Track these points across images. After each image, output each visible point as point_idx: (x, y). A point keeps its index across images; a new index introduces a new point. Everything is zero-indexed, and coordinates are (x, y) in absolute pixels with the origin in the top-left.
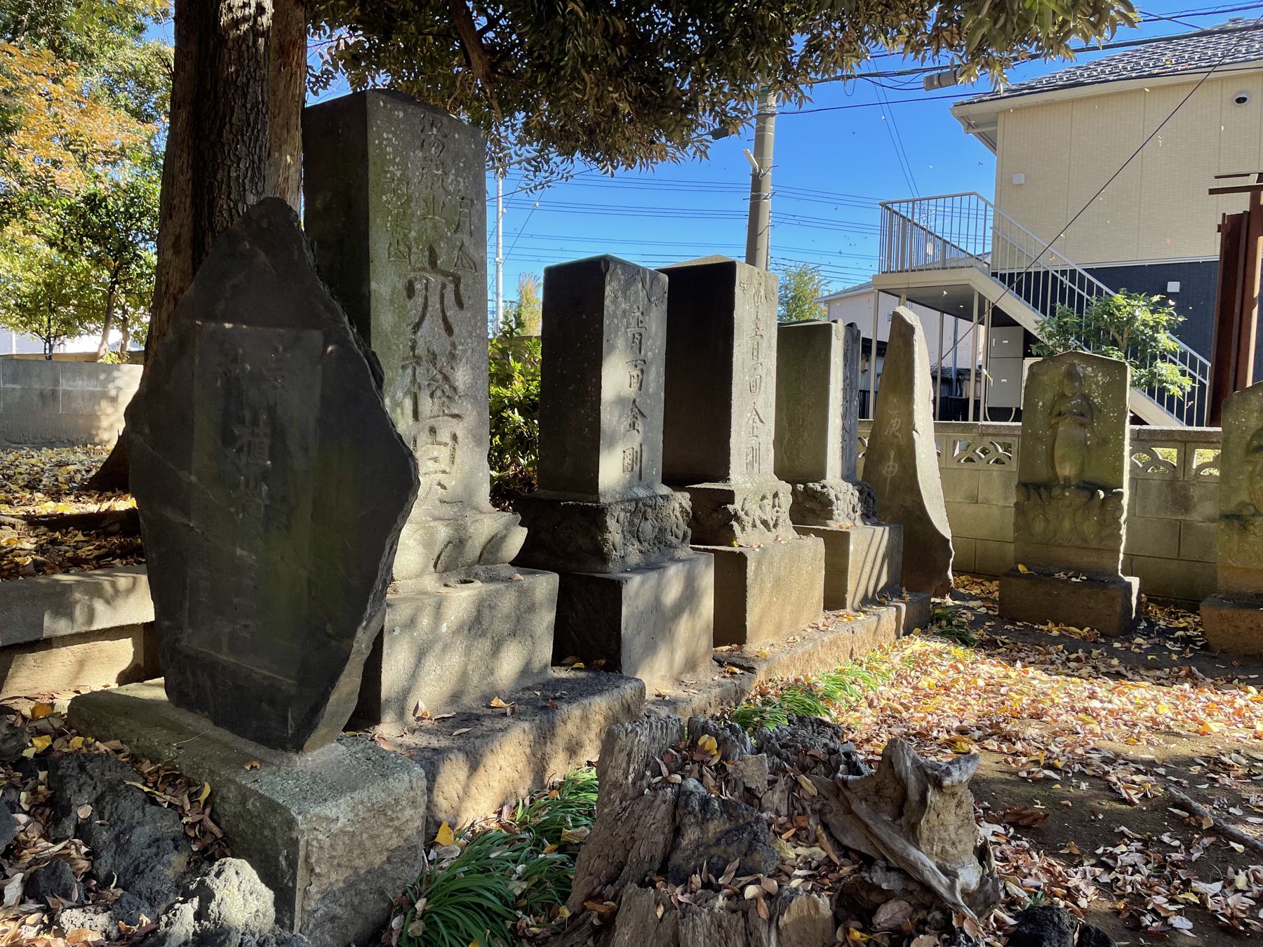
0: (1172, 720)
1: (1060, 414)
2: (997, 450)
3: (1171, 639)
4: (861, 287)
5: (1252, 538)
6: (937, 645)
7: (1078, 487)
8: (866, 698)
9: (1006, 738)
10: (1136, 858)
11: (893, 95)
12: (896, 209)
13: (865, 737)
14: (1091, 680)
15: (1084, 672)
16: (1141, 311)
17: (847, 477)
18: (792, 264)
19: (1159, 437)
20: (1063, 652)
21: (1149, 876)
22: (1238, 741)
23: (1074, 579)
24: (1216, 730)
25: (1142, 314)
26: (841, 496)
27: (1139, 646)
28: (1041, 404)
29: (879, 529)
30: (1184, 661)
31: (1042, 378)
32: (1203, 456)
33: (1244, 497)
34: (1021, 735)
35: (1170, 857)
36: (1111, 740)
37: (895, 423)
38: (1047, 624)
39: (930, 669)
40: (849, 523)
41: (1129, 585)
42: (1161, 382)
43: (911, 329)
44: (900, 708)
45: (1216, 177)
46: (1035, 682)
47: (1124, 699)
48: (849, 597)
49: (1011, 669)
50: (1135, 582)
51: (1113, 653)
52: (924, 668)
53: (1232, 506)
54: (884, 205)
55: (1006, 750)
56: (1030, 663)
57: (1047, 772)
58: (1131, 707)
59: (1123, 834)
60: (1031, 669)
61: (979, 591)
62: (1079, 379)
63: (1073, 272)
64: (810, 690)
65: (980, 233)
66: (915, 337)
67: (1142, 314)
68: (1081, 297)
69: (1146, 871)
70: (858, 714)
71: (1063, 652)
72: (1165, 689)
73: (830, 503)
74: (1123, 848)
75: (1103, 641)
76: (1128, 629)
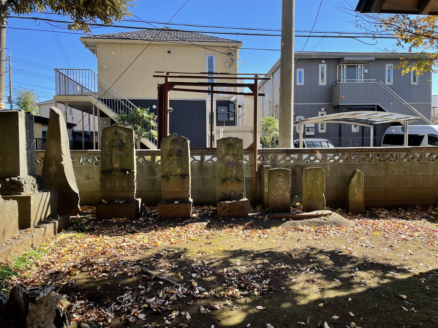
0: (148, 244)
1: (113, 146)
2: (95, 160)
3: (150, 217)
4: (50, 101)
5: (170, 182)
6: (71, 234)
7: (121, 171)
8: (35, 263)
9: (91, 265)
10: (130, 297)
11: (57, 29)
12: (61, 72)
13: (31, 280)
14: (125, 236)
15: (123, 233)
16: (145, 114)
17: (31, 173)
18: (22, 89)
19: (146, 153)
20: (117, 228)
21: (133, 302)
22: (166, 246)
23: (120, 202)
24: (160, 244)
25: (146, 115)
26: (27, 182)
27: (141, 221)
28: (107, 143)
29: (45, 194)
30: (154, 223)
31: (106, 134)
32: (158, 158)
33: (167, 170)
34: (96, 262)
35: (140, 293)
36: (127, 256)
37: (54, 152)
38: (112, 219)
39: (66, 245)
40: (32, 192)
41: (138, 201)
42: (153, 136)
43: (58, 116)
44: (50, 263)
45: (156, 72)
46: (105, 241)
47: (134, 240)
48: (32, 223)
49: (98, 238)
50: (140, 200)
51: (133, 225)
52: (64, 245)
53: (165, 173)
54: (55, 69)
55: (90, 270)
56: (105, 234)
57: (103, 274)
58: (135, 242)
59: (126, 289)
60: (105, 236)
61: (91, 211)
62: (119, 134)
63: (125, 100)
64: (7, 267)
65: (93, 84)
66: (60, 119)
67: (146, 115)
68: (128, 108)
69: (132, 301)
70: (30, 271)
71: (117, 228)
72: (147, 234)
73: (22, 185)
74: (126, 294)
75: (130, 221)
76: (138, 215)
